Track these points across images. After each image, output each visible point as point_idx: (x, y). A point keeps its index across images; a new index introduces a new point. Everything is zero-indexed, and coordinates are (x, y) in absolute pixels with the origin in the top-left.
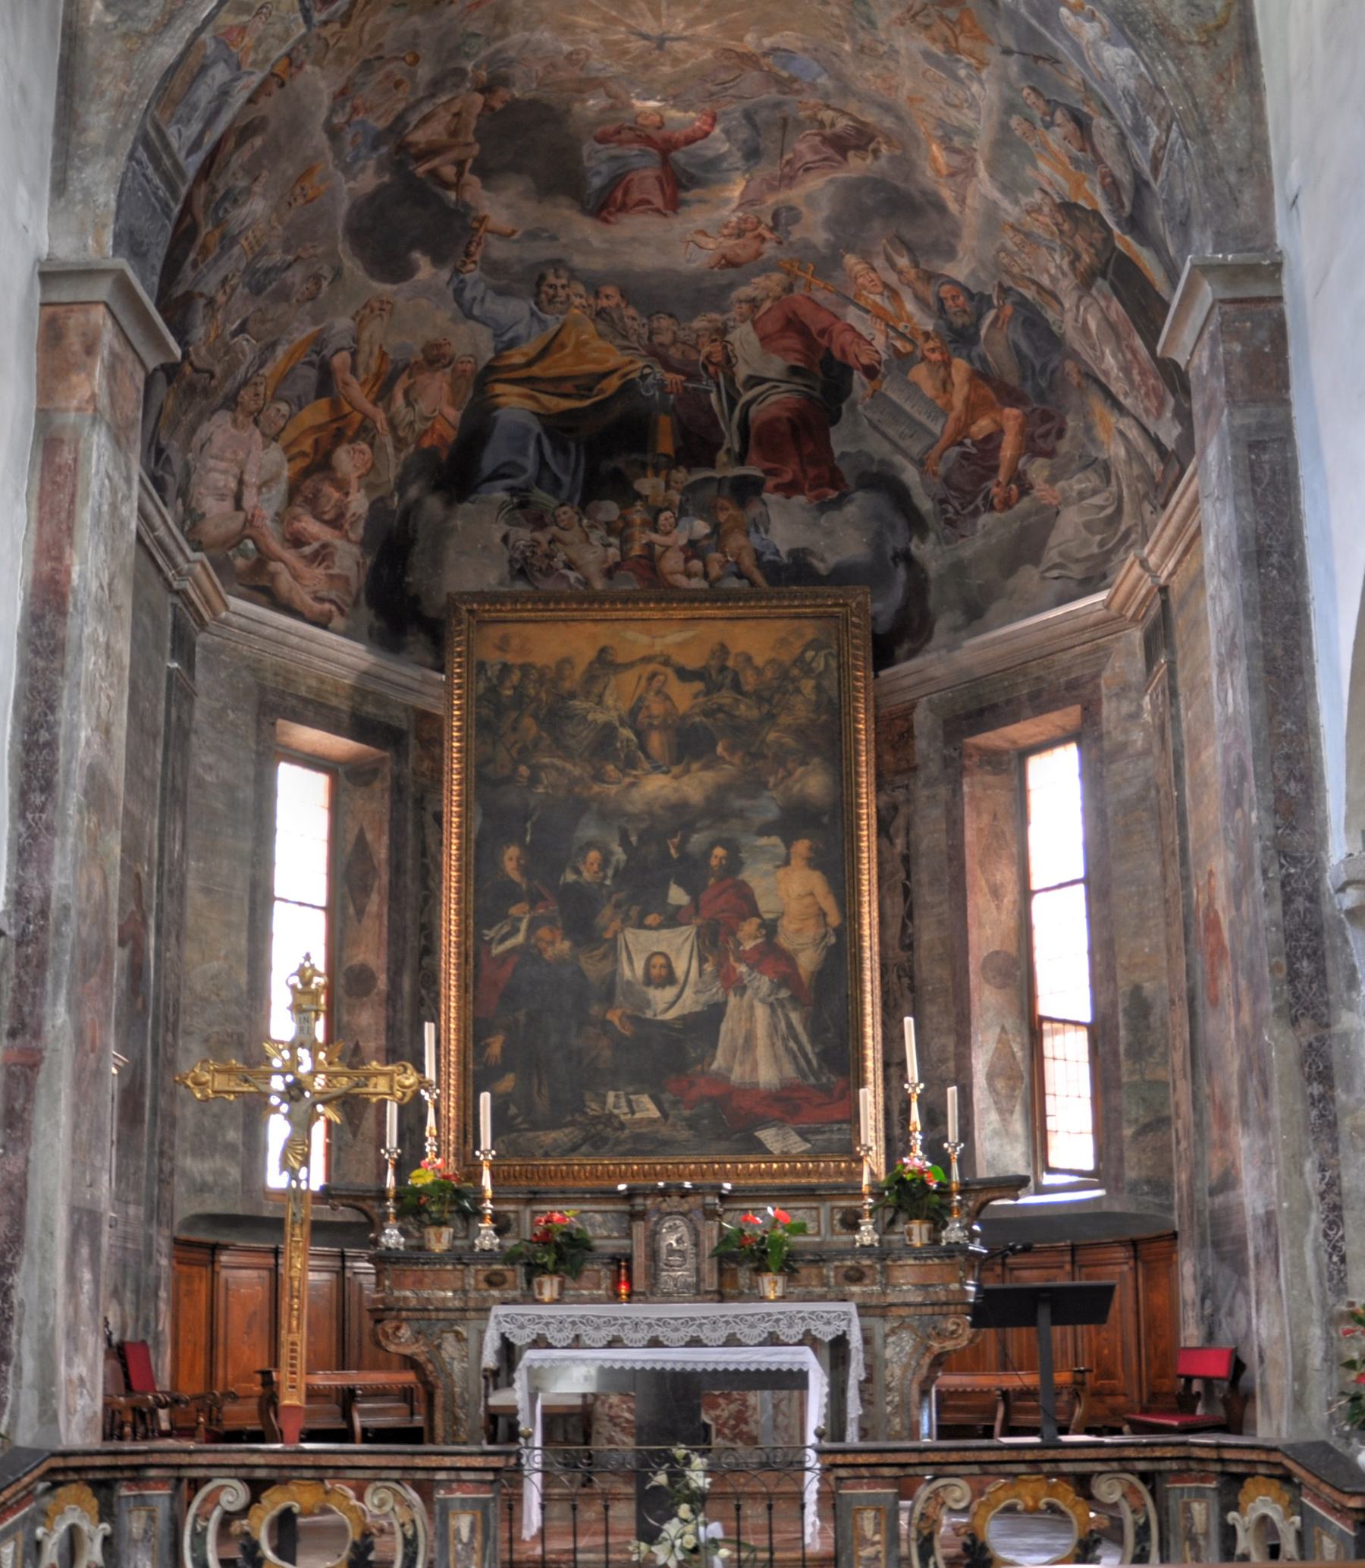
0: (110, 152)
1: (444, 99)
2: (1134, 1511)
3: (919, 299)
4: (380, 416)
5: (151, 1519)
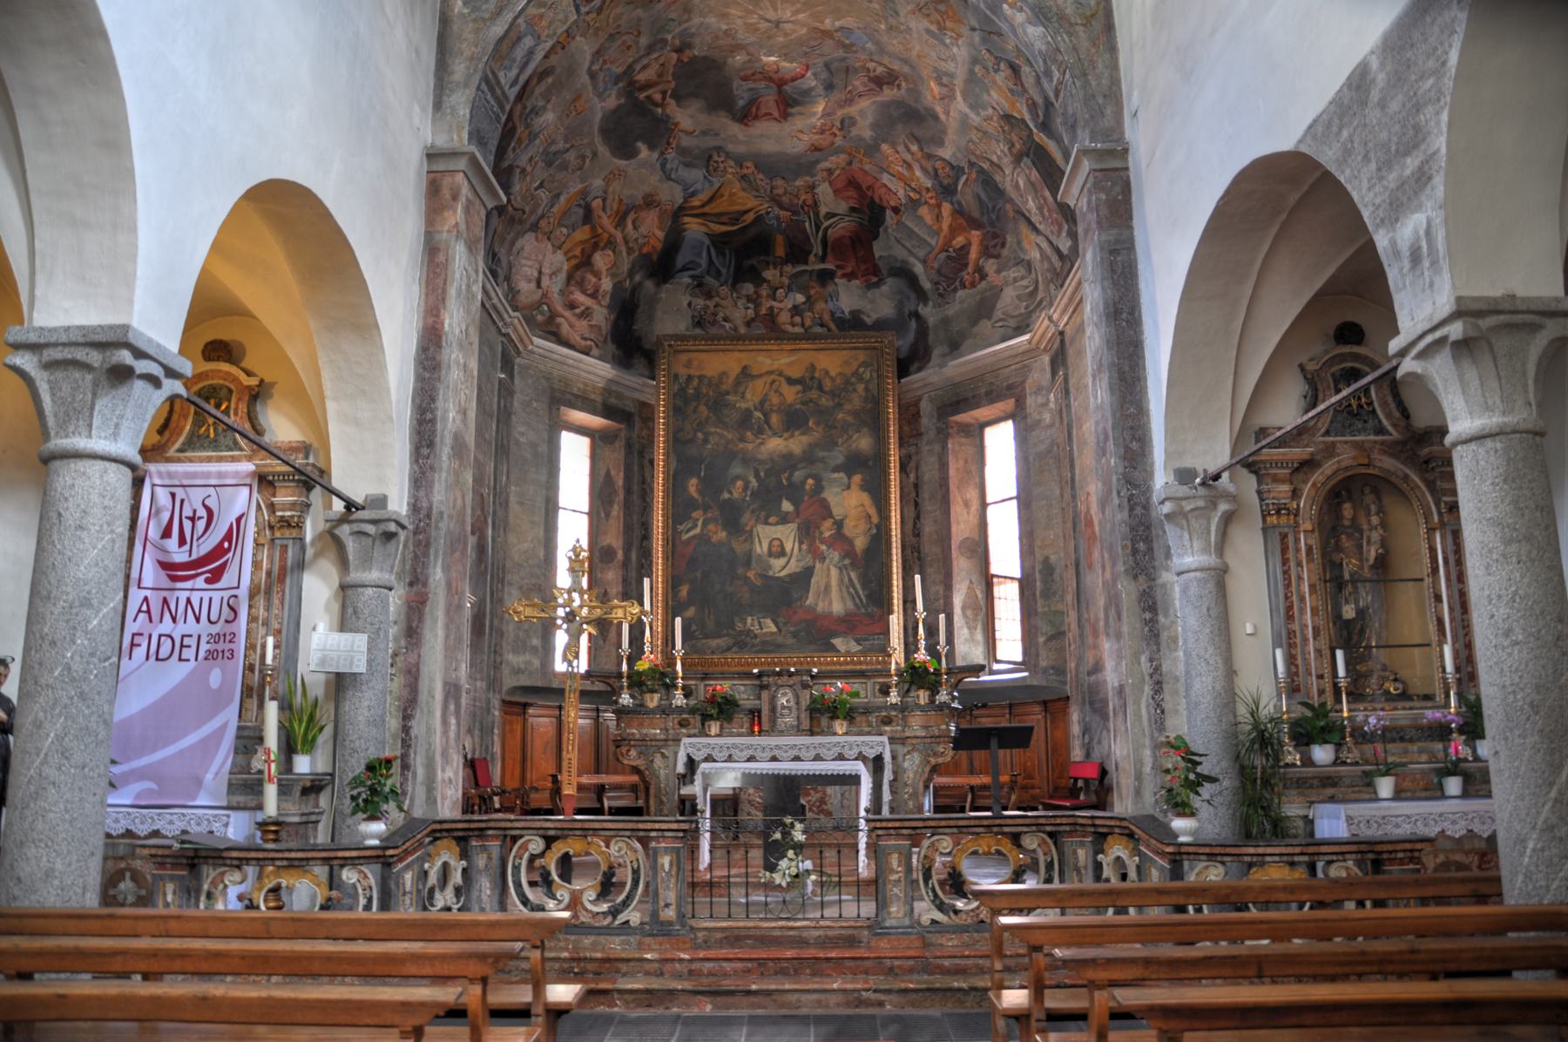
0: (466, 86)
1: (655, 56)
2: (1045, 854)
3: (923, 169)
4: (619, 235)
5: (490, 858)
